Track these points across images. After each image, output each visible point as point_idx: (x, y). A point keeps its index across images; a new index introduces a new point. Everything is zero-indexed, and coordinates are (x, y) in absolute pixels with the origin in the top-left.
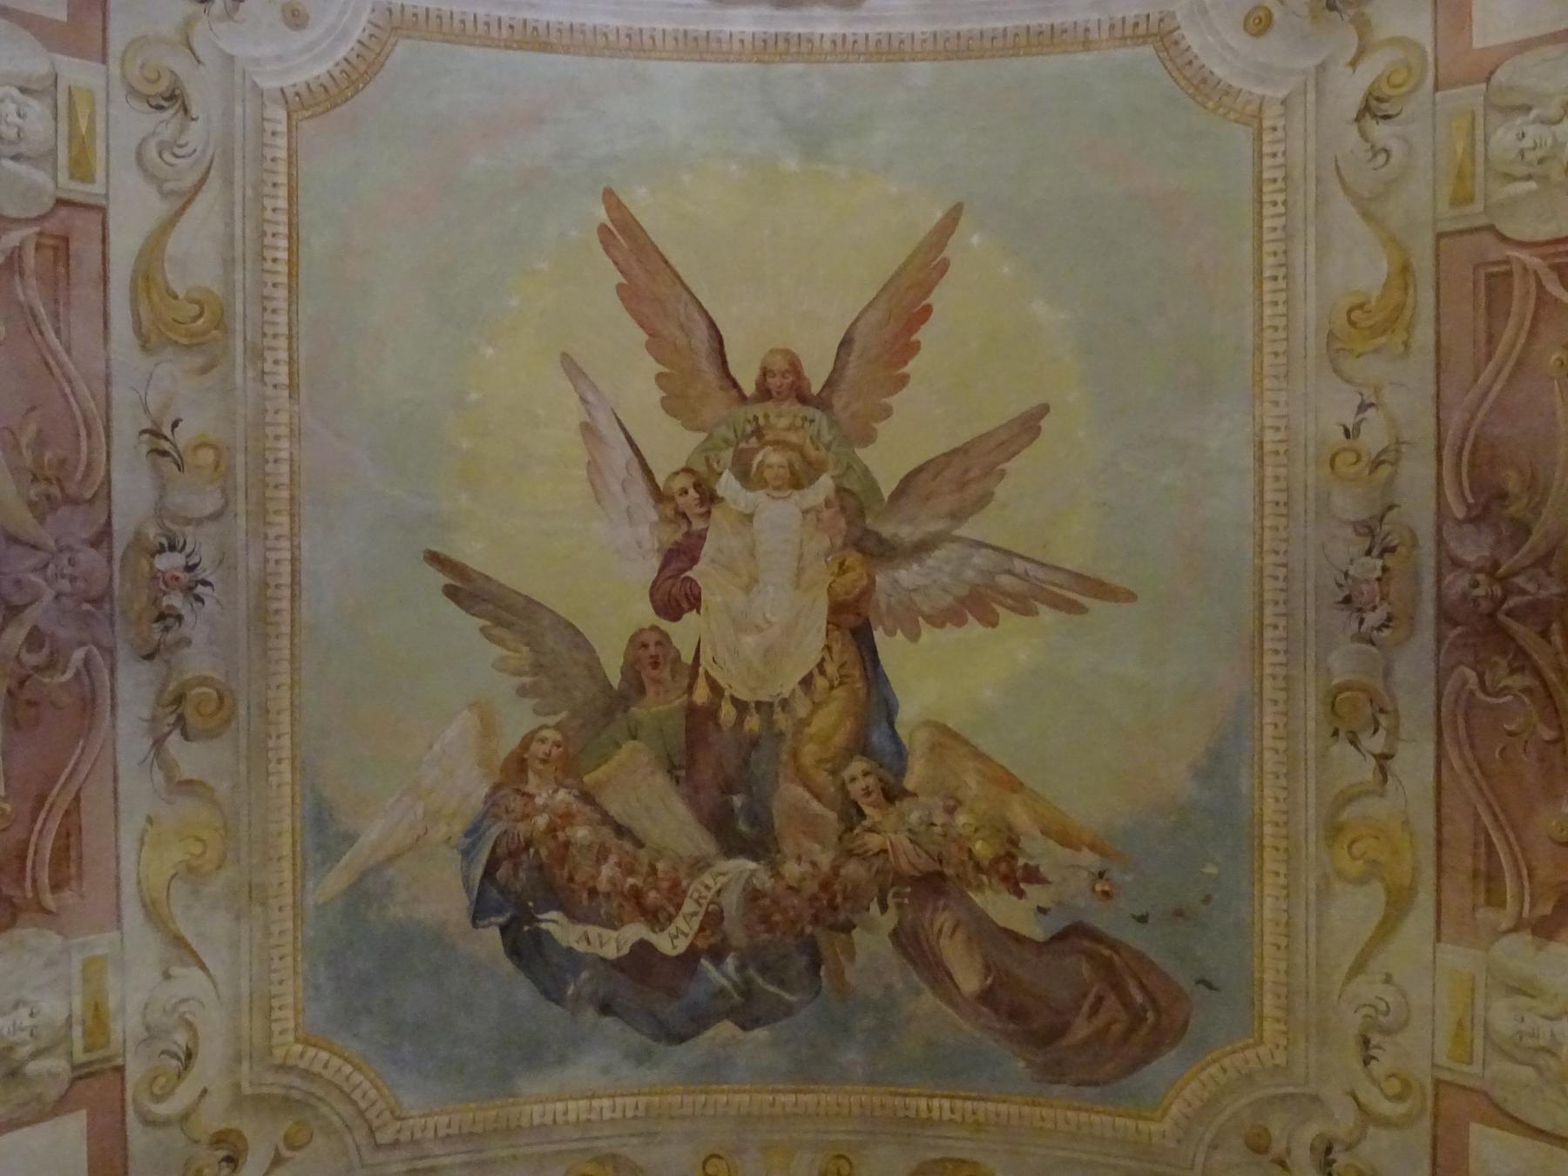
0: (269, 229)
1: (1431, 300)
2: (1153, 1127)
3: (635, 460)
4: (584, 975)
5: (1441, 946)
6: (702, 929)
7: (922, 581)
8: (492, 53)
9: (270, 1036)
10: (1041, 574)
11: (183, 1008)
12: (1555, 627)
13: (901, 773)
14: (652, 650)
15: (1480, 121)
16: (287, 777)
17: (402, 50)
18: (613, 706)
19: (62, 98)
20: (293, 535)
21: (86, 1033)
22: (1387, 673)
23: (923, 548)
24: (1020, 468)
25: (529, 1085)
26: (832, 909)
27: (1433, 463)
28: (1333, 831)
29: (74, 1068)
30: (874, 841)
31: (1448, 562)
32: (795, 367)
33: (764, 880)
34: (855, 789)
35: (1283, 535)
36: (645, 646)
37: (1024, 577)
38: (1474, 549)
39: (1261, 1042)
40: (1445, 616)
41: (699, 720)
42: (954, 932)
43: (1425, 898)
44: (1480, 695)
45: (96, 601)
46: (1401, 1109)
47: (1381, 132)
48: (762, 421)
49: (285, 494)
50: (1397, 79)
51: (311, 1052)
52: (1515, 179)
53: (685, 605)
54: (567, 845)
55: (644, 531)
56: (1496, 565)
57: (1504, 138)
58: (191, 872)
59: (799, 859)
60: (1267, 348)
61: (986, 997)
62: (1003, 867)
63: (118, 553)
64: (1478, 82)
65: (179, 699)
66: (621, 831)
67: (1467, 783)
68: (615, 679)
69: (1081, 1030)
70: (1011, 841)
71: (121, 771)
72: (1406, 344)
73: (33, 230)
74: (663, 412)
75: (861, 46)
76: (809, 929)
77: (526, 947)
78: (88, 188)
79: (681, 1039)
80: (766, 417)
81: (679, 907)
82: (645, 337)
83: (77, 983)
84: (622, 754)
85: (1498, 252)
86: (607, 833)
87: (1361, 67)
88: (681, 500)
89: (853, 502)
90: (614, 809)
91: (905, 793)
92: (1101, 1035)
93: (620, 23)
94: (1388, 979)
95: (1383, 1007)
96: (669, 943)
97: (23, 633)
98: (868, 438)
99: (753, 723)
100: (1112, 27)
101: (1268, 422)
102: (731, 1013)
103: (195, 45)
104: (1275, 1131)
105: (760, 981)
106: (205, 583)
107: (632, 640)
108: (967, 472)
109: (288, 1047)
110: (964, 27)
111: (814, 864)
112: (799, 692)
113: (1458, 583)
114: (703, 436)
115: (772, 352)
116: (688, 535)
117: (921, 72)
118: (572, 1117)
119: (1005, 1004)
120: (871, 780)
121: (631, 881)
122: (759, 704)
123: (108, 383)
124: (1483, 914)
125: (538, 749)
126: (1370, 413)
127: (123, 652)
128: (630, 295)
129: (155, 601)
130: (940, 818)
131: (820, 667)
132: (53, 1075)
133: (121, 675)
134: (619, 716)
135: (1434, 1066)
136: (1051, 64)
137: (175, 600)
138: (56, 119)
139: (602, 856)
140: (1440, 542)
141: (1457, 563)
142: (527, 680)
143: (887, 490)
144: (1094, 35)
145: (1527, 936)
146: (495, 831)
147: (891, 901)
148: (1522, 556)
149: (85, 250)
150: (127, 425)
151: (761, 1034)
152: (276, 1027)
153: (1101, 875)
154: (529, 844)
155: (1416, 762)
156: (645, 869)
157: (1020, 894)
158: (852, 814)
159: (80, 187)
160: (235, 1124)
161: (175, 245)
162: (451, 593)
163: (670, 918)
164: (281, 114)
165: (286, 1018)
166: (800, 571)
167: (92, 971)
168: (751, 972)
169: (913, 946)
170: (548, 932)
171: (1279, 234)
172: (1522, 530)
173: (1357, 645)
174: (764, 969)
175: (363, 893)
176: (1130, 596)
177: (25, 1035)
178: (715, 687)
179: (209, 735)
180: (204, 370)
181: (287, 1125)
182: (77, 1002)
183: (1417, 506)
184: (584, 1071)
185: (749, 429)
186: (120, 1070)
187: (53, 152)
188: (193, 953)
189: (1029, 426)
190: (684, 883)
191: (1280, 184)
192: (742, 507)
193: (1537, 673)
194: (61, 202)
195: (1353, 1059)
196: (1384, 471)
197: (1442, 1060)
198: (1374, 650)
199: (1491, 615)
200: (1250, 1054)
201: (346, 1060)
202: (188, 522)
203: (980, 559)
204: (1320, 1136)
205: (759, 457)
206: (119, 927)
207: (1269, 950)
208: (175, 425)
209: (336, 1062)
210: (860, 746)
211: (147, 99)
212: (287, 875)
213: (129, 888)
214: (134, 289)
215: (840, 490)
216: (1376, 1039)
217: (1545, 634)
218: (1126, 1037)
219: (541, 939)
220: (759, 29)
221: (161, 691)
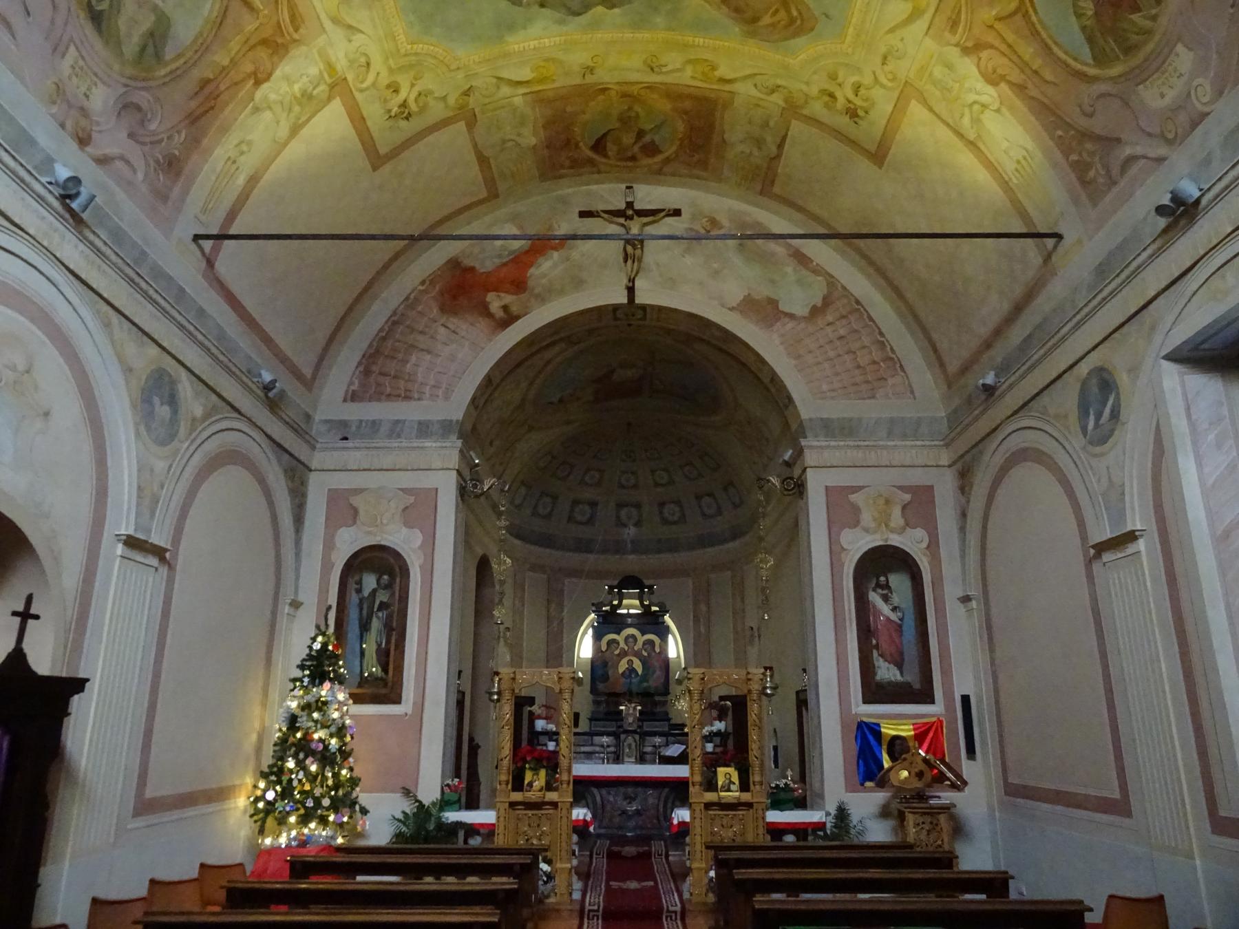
25: (510, 39)
46: (890, 84)
69: (767, 20)
79: (579, 14)
92: (773, 25)
94: (902, 40)
109: (405, 47)
124: (947, 34)
151: (616, 10)
160: (393, 79)
165: (402, 38)
167: (322, 53)
181: (412, 73)
184: (536, 29)
186: (345, 79)
195: (879, 60)
213: (323, 16)
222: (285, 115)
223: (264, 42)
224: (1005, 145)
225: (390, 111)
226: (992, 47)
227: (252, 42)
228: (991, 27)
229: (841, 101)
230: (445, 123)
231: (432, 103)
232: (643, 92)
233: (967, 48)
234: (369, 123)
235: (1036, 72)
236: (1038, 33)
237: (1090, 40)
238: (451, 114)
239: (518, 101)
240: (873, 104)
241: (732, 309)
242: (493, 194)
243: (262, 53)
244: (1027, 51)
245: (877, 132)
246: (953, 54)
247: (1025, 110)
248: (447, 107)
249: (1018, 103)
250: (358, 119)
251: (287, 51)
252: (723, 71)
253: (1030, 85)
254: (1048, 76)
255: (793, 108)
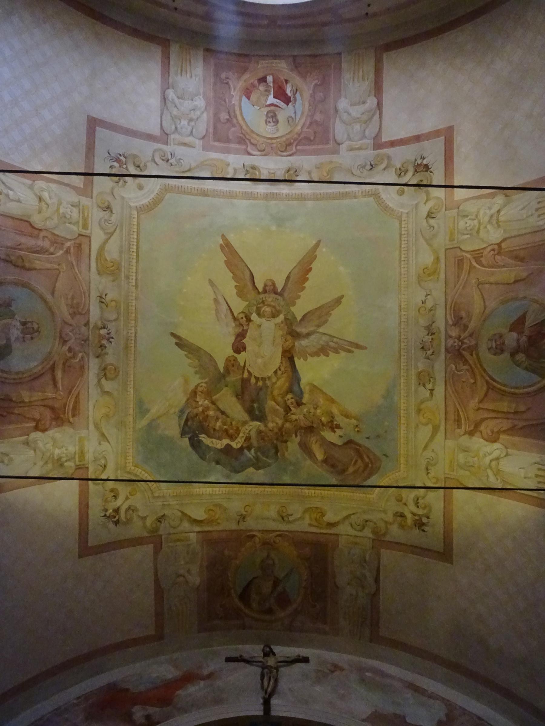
0: (132, 243)
1: (444, 267)
2: (370, 496)
3: (228, 308)
4: (212, 453)
5: (447, 441)
6: (245, 441)
7: (308, 344)
8: (192, 197)
9: (126, 463)
10: (342, 342)
11: (104, 453)
12: (474, 352)
13: (302, 398)
14: (232, 362)
15: (456, 218)
16: (132, 392)
17: (168, 196)
18: (220, 378)
19: (81, 207)
20: (136, 326)
21: (80, 457)
22: (433, 367)
23: (308, 335)
24: (336, 313)
26: (282, 436)
27: (444, 310)
28: (419, 411)
29: (76, 466)
30: (294, 417)
31: (448, 336)
32: (274, 284)
33: (262, 428)
34: (289, 403)
35: (406, 330)
36: (230, 361)
37: (337, 343)
38: (454, 332)
39: (400, 471)
40: (447, 351)
41: (245, 382)
42: (316, 442)
43: (442, 428)
44: (456, 372)
45: (85, 341)
47: (432, 222)
48: (264, 299)
49: (133, 315)
50: (436, 208)
51: (137, 469)
52: (464, 234)
53: (242, 350)
54: (207, 416)
55: (231, 329)
56: (460, 336)
57: (462, 224)
58: (107, 416)
59: (273, 422)
60: (403, 279)
61: (325, 461)
62: (330, 424)
63: (91, 328)
64: (455, 209)
65: (105, 369)
66: (223, 413)
67: (453, 395)
68: (222, 371)
69: (351, 469)
70: (332, 417)
71: (90, 387)
72: (438, 278)
73: (73, 242)
74: (236, 296)
75: (294, 196)
76: (275, 442)
77: (196, 444)
78: (87, 232)
79: (238, 472)
80: (265, 298)
81: (238, 435)
82: (232, 275)
83: (77, 443)
84: (223, 392)
85: (459, 253)
86: (219, 413)
87: (427, 204)
88: (241, 321)
89: (289, 322)
90: (221, 407)
91: (303, 404)
92: (355, 472)
93: (228, 189)
94: (433, 451)
95: (431, 458)
96: (235, 445)
97: (67, 348)
98: (294, 304)
99: (260, 383)
100: (362, 192)
101: (403, 300)
102: (253, 465)
103: (115, 195)
104: (404, 496)
105: (261, 456)
106: (113, 338)
107: (226, 360)
108: (321, 314)
110: (322, 192)
111: (277, 423)
112: (273, 375)
113: (450, 342)
114: (247, 303)
115: (267, 280)
116: (243, 330)
117: (310, 204)
118: (208, 493)
119: (329, 462)
120: (293, 400)
121: (225, 427)
122: (262, 378)
123: (90, 282)
124: (458, 431)
125: (200, 389)
126: (429, 297)
127: (91, 354)
128: (228, 264)
129: (99, 342)
130: (312, 411)
131: (279, 368)
132: (71, 467)
133: (90, 361)
134: (223, 380)
135: (445, 474)
136: (346, 202)
137: (104, 342)
138: (79, 212)
139: (217, 419)
140: (446, 331)
141: (451, 337)
142: (197, 369)
143: (299, 318)
144: (357, 194)
145: (467, 436)
146: (187, 412)
147: (298, 434)
148: (466, 334)
149: (85, 247)
150: (94, 294)
151: (261, 471)
152: (128, 461)
153: (357, 426)
154: (197, 415)
155: (440, 390)
156: (229, 423)
157: (335, 432)
158: (288, 410)
159: (84, 231)
161: (107, 247)
162: (177, 344)
163: (236, 438)
164: (136, 213)
165: (130, 459)
166: (274, 341)
167: (81, 440)
168: (259, 454)
169: (305, 447)
170: (202, 440)
171: (406, 249)
172: (466, 327)
173: (426, 360)
174: (263, 453)
175: (151, 427)
176: (366, 348)
177: (64, 455)
178: (250, 373)
179: (112, 379)
180: (114, 281)
182: (77, 448)
183: (440, 323)
185: (261, 301)
186: (87, 468)
187: (78, 222)
188: (107, 439)
189: (338, 301)
190: (240, 428)
191: (406, 236)
192: (258, 323)
193: (470, 365)
194: (80, 235)
196: (432, 312)
197: (447, 472)
198: (429, 361)
199: (458, 350)
200: (397, 474)
201: (146, 472)
202: (109, 321)
203: (325, 338)
204: (416, 495)
205: (263, 309)
206: (88, 429)
207: (402, 445)
208: (106, 295)
209: (143, 472)
210: (290, 390)
211: (102, 208)
212: (131, 419)
214: (97, 259)
215: (286, 319)
216: (430, 468)
217: (472, 355)
218: (363, 471)
219: (200, 442)
220: (265, 191)
221: (100, 366)
222: (41, 463)
223: (52, 409)
224: (522, 473)
225: (106, 510)
226: (485, 419)
227: (46, 402)
228: (479, 409)
229: (409, 516)
230: (137, 541)
231: (135, 518)
232: (278, 540)
233: (471, 431)
234: (90, 512)
235: (516, 413)
236: (505, 391)
237: (533, 371)
238: (146, 534)
239: (193, 536)
240: (430, 510)
241: (363, 720)
242: (159, 637)
243: (48, 414)
244: (504, 406)
245: (440, 528)
246: (465, 440)
247: (522, 439)
248: (144, 526)
249: (516, 439)
250: (84, 506)
251: (62, 425)
252: (330, 517)
253: (516, 422)
254: (522, 408)
255: (380, 541)
